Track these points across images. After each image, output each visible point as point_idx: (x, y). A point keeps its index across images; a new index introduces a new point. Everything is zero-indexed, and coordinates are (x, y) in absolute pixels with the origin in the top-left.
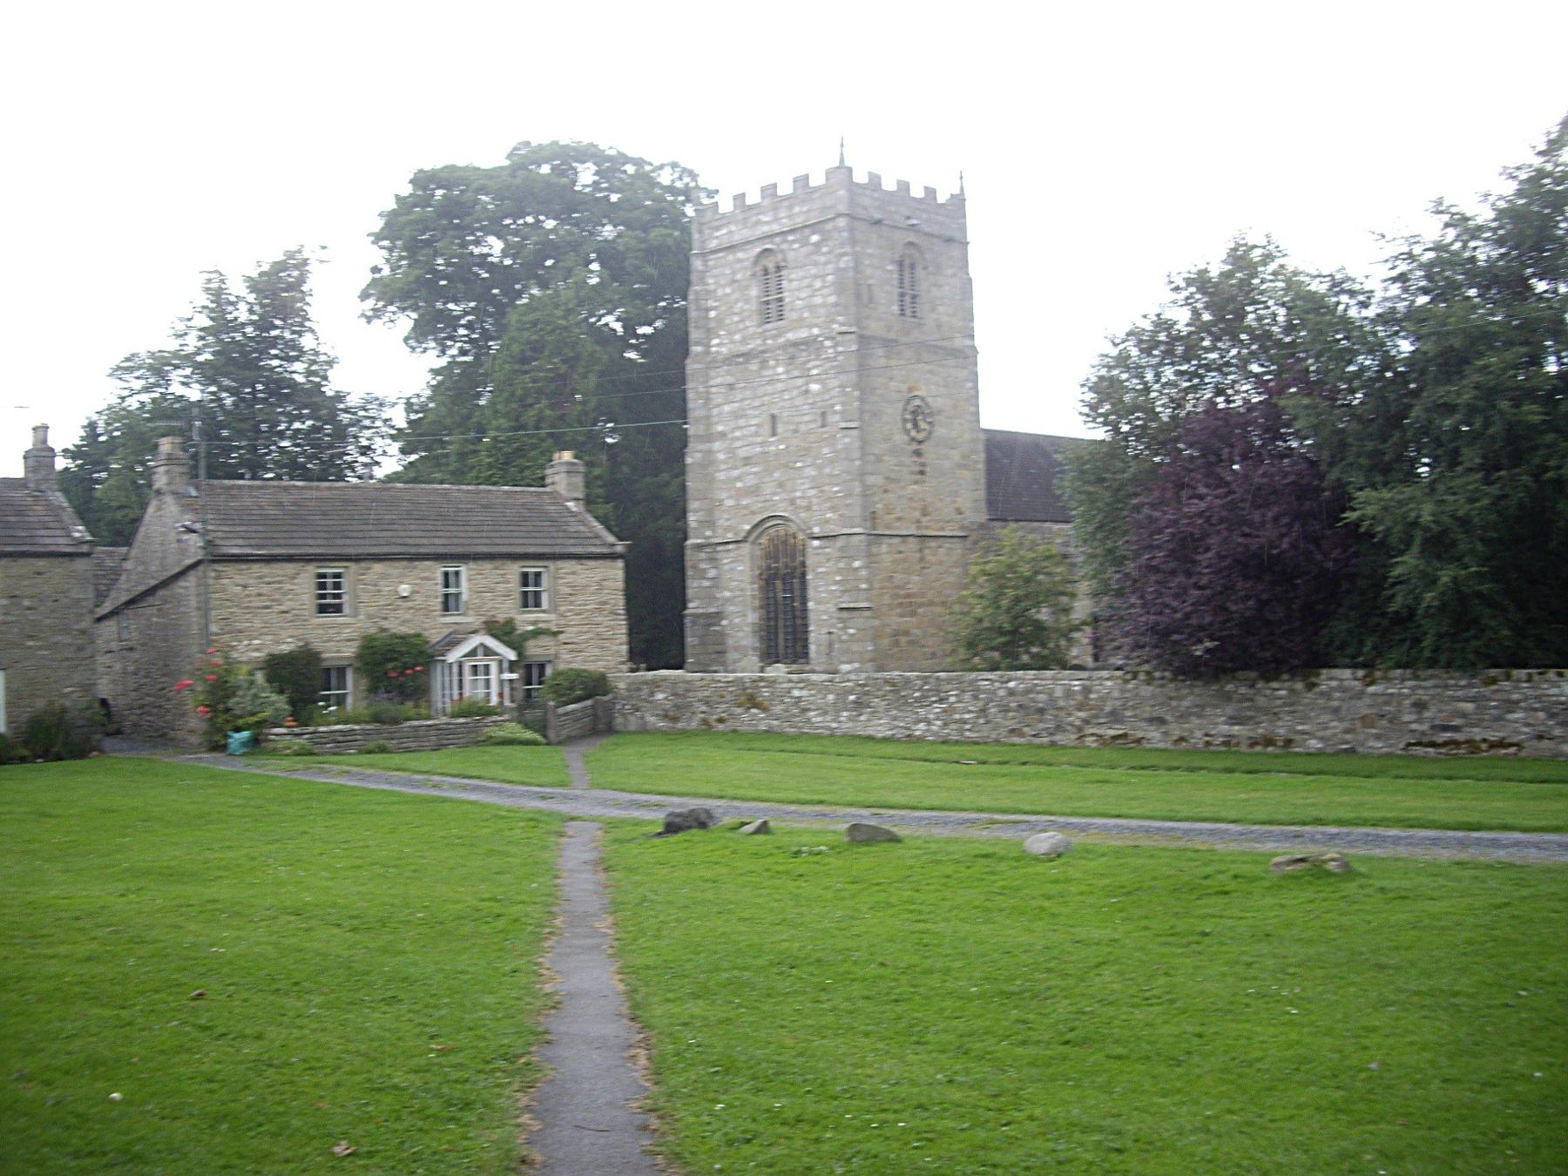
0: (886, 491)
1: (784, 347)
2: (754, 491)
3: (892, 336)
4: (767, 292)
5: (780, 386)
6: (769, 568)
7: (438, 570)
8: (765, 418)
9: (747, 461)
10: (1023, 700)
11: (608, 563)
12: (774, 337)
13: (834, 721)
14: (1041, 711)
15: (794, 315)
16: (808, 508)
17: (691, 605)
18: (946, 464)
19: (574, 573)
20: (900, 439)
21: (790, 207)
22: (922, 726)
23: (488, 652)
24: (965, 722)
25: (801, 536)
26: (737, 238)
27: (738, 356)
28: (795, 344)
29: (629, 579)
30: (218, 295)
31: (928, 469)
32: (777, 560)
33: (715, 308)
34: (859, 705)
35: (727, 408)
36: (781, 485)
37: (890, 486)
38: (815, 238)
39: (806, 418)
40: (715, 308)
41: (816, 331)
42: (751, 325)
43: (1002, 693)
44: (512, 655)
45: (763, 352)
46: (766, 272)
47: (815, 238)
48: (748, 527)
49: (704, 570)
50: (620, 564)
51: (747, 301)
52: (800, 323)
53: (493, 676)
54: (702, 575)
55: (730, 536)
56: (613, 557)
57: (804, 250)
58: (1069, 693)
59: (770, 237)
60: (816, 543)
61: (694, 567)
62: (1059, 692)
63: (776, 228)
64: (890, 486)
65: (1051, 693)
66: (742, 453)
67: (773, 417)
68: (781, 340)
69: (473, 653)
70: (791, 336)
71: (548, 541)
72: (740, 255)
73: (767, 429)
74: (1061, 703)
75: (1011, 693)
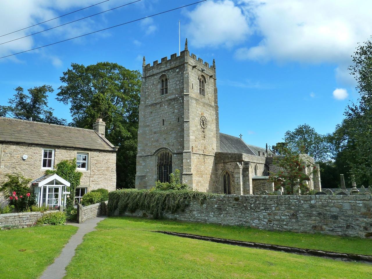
0: (195, 141)
1: (167, 101)
2: (157, 141)
3: (197, 98)
4: (163, 86)
5: (166, 111)
6: (160, 163)
7: (42, 151)
8: (161, 120)
9: (155, 133)
10: (320, 211)
11: (111, 154)
12: (164, 98)
13: (207, 216)
14: (335, 217)
15: (170, 92)
16: (173, 145)
17: (137, 173)
18: (210, 136)
19: (98, 156)
20: (199, 127)
21: (170, 63)
22: (256, 221)
23: (58, 183)
24: (283, 221)
25: (170, 153)
26: (155, 73)
27: (154, 104)
28: (170, 100)
29: (118, 160)
30: (22, 97)
31: (205, 137)
32: (163, 160)
33: (147, 92)
34: (219, 209)
35: (150, 118)
36: (165, 139)
37: (197, 140)
38: (177, 70)
39: (173, 120)
40: (147, 92)
41: (177, 95)
42: (158, 95)
43: (306, 206)
44: (68, 184)
45: (160, 102)
46: (163, 81)
47: (177, 70)
48: (154, 151)
49: (142, 163)
50: (115, 154)
51: (157, 89)
52: (172, 94)
53: (60, 193)
54: (141, 165)
55: (149, 154)
56: (112, 152)
57: (174, 74)
58: (354, 208)
59: (164, 71)
60: (175, 155)
61: (139, 162)
62: (347, 206)
63: (166, 69)
64: (197, 140)
65: (341, 208)
66: (155, 130)
67: (163, 120)
68: (167, 99)
69: (51, 183)
70: (169, 98)
71: (89, 145)
72: (156, 77)
73: (162, 123)
74: (350, 213)
75: (312, 206)
